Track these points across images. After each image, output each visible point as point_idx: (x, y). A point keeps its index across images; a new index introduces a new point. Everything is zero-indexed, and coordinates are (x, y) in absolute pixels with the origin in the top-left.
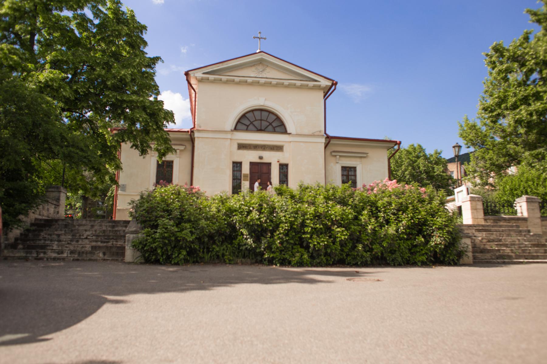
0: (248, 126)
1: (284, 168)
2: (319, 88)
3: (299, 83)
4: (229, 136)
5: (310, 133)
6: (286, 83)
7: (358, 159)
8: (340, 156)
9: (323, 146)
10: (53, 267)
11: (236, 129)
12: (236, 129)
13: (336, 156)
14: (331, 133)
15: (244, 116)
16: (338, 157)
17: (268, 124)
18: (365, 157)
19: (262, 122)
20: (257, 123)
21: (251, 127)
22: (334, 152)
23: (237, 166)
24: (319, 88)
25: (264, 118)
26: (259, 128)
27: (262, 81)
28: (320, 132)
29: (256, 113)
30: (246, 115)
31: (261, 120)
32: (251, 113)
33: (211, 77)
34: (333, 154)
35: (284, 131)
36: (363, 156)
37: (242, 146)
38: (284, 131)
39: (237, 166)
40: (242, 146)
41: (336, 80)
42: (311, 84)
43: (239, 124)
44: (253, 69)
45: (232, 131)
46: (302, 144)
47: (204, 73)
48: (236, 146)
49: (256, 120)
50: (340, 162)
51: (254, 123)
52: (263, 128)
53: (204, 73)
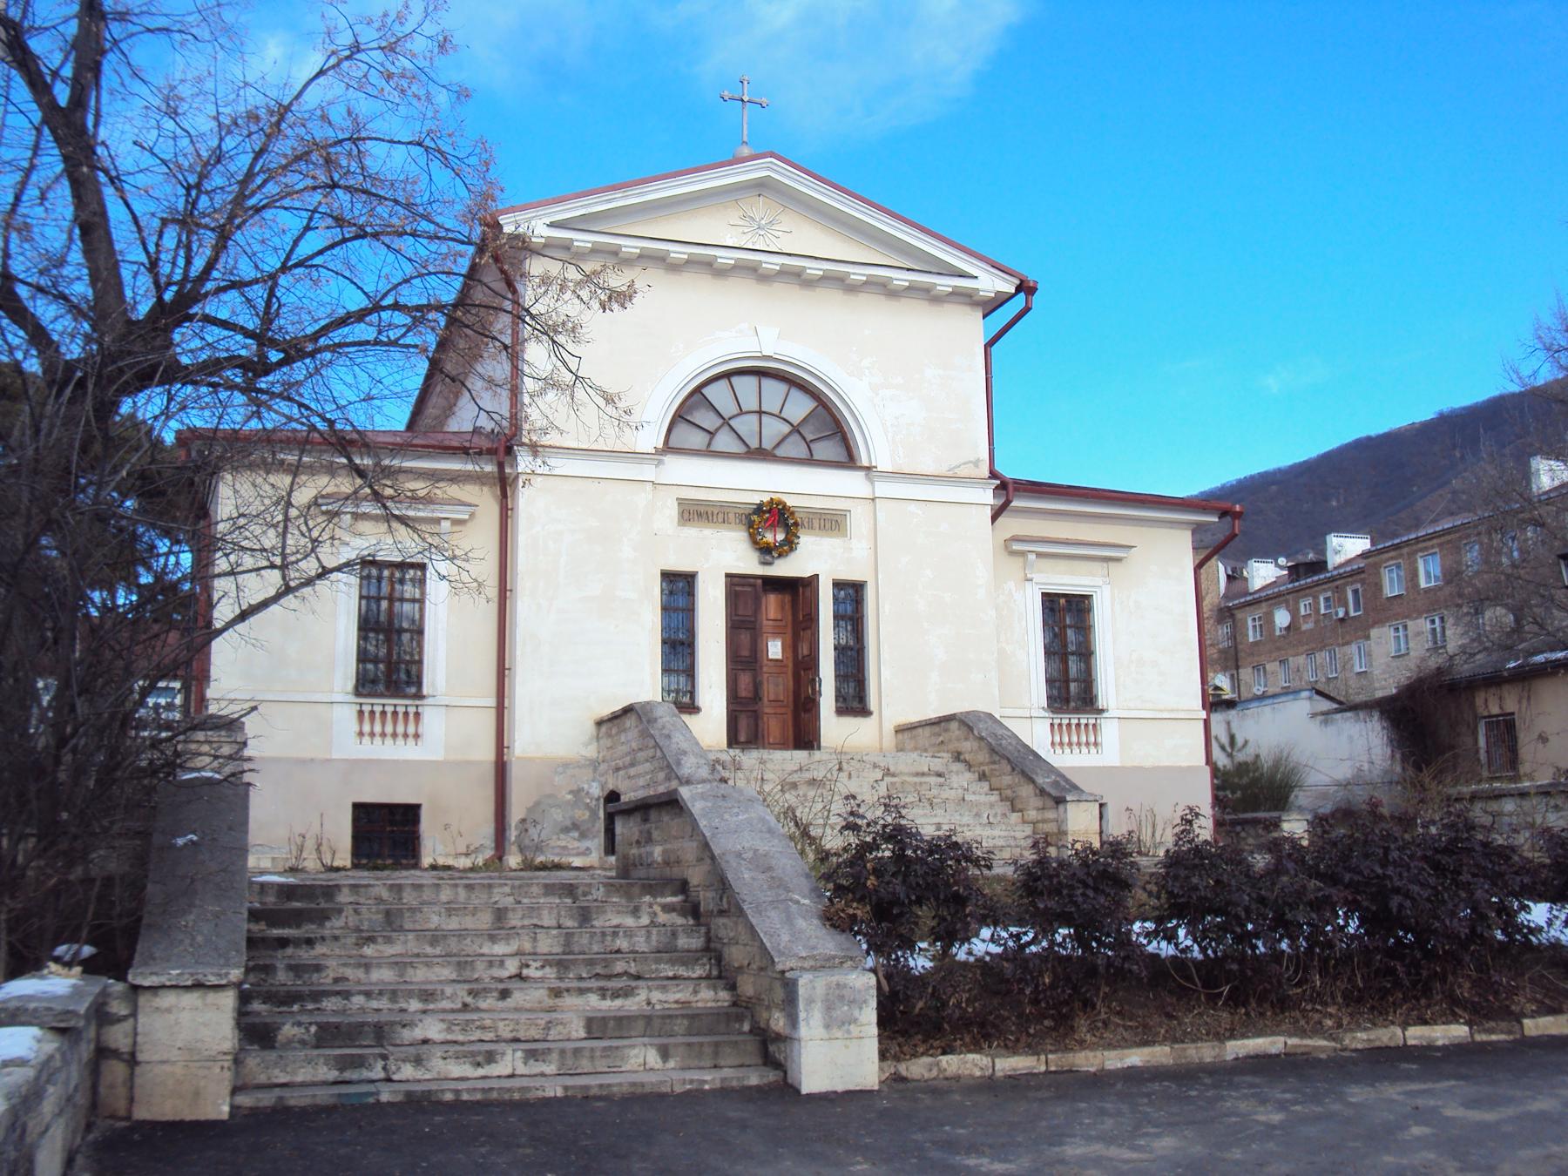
0: (712, 434)
1: (852, 594)
2: (967, 298)
3: (901, 279)
4: (648, 472)
5: (943, 470)
6: (858, 274)
7: (1097, 566)
8: (1039, 555)
9: (988, 513)
10: (1100, 1081)
11: (669, 448)
12: (669, 448)
13: (1023, 554)
14: (1009, 472)
15: (696, 397)
16: (446, 525)
17: (786, 429)
18: (1118, 560)
19: (765, 418)
20: (746, 425)
21: (724, 441)
22: (1016, 539)
23: (679, 588)
24: (967, 298)
25: (772, 404)
26: (754, 444)
27: (772, 263)
28: (976, 463)
29: (745, 385)
30: (705, 391)
31: (760, 413)
32: (723, 383)
33: (583, 240)
34: (1016, 547)
35: (849, 460)
36: (1110, 556)
37: (695, 512)
38: (849, 460)
39: (679, 588)
40: (695, 512)
41: (1031, 276)
42: (945, 284)
43: (682, 428)
44: (734, 216)
45: (659, 452)
46: (912, 507)
47: (552, 225)
48: (673, 511)
49: (742, 413)
50: (1037, 577)
51: (732, 422)
52: (767, 445)
53: (552, 225)
